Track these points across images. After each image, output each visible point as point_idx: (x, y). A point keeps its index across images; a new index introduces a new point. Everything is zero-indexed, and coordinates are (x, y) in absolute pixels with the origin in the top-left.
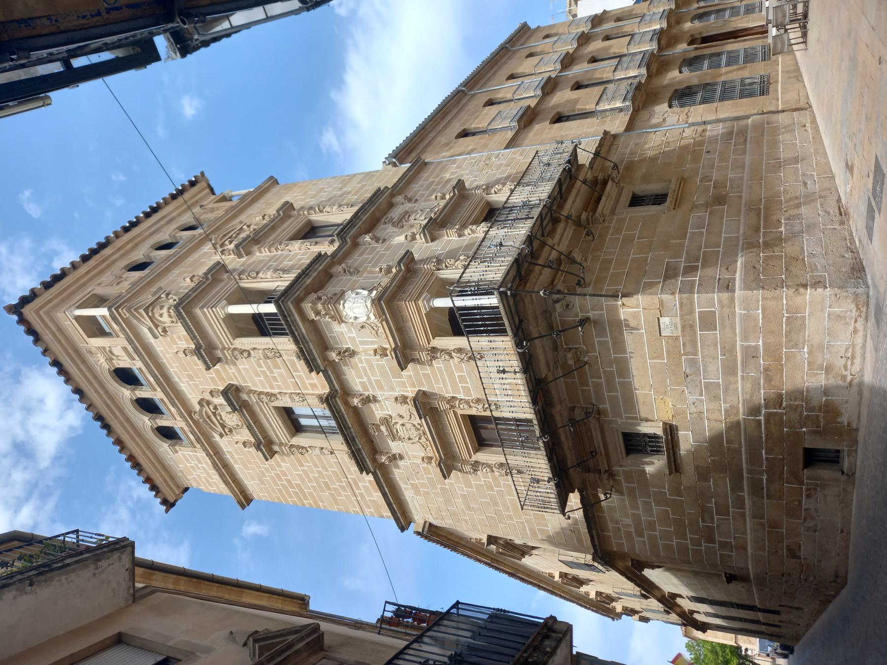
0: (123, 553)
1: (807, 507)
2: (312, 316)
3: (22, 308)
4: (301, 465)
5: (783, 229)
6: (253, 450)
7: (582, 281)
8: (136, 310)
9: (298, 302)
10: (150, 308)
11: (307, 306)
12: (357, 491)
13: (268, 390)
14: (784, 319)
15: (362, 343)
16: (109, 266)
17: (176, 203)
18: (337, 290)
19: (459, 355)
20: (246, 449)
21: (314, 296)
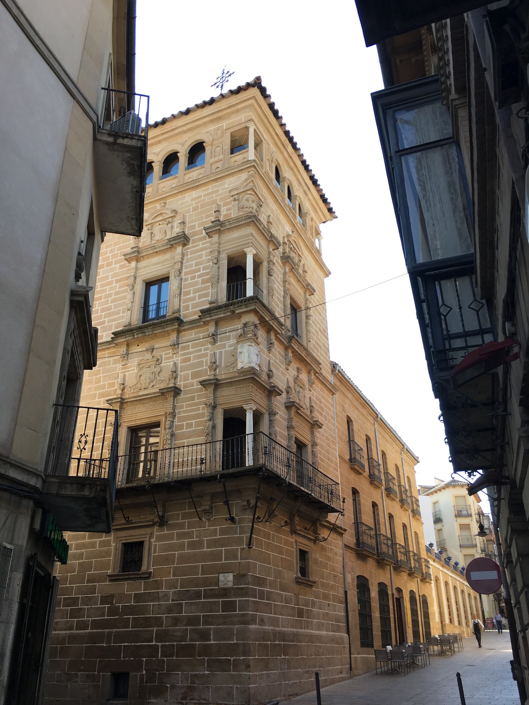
0: (136, 231)
1: (252, 663)
3: (258, 88)
4: (117, 281)
5: (283, 657)
7: (260, 520)
9: (255, 311)
10: (253, 193)
13: (184, 271)
14: (229, 658)
16: (279, 149)
17: (317, 197)
19: (210, 426)
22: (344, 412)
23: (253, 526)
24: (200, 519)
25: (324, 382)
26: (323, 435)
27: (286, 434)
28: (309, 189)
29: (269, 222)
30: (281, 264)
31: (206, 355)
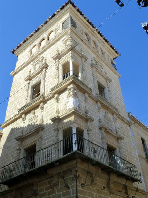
2: (69, 87)
3: (71, 4)
6: (28, 74)
8: (70, 35)
11: (72, 86)
12: (14, 109)
15: (61, 105)
17: (109, 47)
18: (79, 96)
19: (56, 140)
20: (28, 73)
21: (76, 88)
22: (139, 135)
23: (77, 189)
24: (53, 189)
25: (123, 119)
26: (126, 144)
27: (53, 101)
28: (104, 44)
29: (81, 51)
30: (90, 68)
31: (54, 108)
